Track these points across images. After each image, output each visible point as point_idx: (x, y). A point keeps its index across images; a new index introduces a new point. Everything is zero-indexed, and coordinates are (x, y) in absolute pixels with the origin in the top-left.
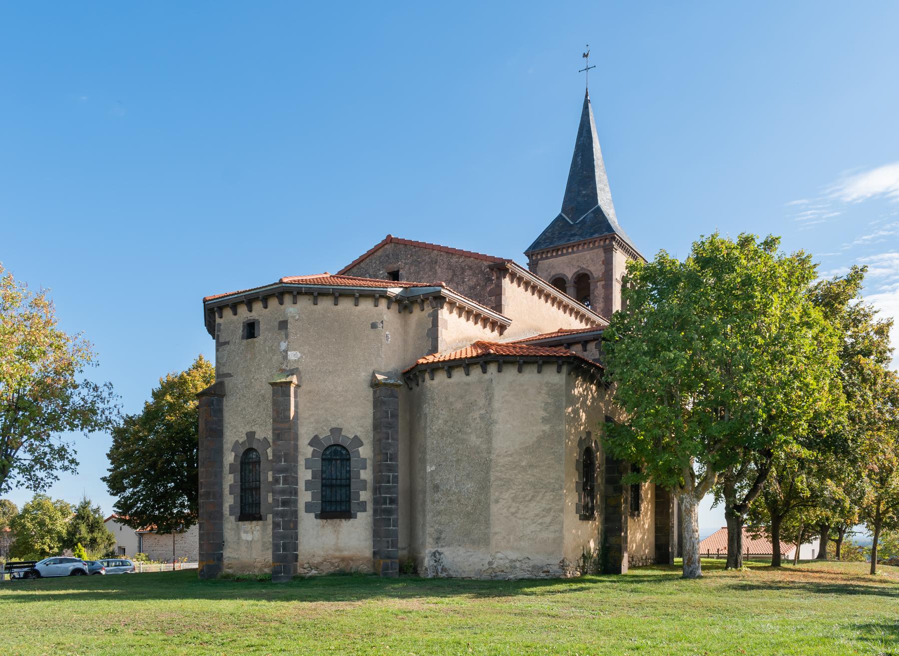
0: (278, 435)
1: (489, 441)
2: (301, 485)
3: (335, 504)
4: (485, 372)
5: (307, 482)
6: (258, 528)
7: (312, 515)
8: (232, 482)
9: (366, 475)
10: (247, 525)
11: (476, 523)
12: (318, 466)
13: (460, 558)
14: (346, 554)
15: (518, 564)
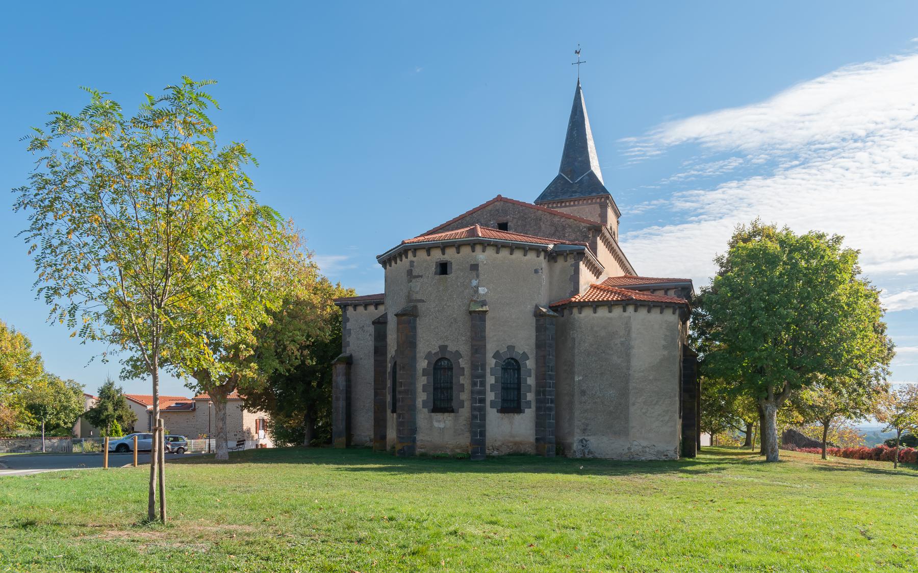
0: (476, 350)
1: (629, 361)
2: (488, 388)
3: (511, 404)
4: (625, 311)
5: (492, 385)
6: (450, 418)
7: (495, 410)
8: (425, 382)
9: (531, 381)
10: (439, 416)
11: (617, 417)
12: (499, 373)
13: (603, 444)
14: (517, 439)
15: (647, 450)
